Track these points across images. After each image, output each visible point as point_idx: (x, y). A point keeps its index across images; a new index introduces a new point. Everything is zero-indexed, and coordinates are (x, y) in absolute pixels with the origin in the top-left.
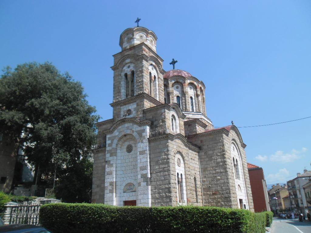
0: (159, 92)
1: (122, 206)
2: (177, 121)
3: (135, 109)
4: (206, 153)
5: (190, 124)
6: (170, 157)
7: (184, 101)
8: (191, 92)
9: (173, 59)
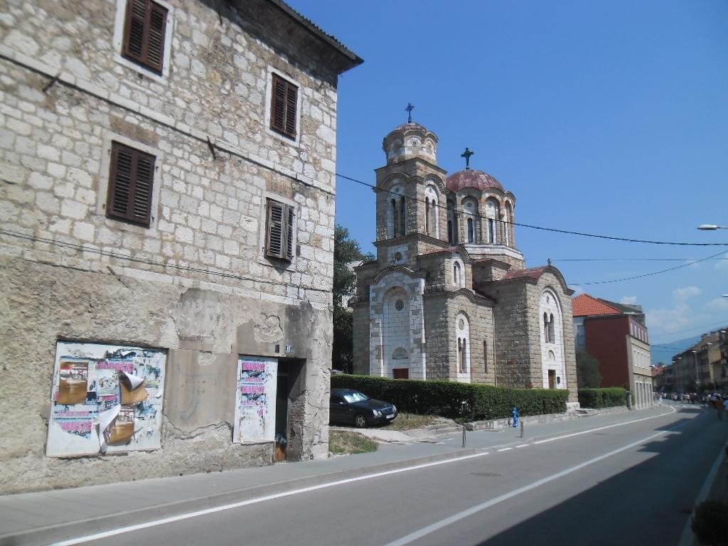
0: (439, 223)
1: (391, 378)
2: (463, 268)
3: (406, 253)
4: (502, 308)
5: (481, 267)
6: (448, 319)
7: (478, 226)
8: (489, 211)
9: (467, 149)
